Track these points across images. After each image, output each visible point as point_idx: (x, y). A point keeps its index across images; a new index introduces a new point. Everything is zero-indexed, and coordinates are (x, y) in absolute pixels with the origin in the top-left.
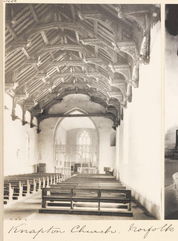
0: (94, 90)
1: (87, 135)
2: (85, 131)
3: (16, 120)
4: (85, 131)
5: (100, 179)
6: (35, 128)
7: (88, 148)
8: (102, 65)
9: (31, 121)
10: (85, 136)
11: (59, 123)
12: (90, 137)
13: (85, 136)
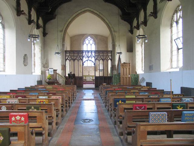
0: (135, 23)
1: (91, 42)
2: (89, 37)
3: (22, 16)
4: (89, 37)
5: (75, 17)
6: (41, 29)
7: (94, 54)
8: (178, 108)
9: (37, 21)
10: (89, 43)
11: (65, 30)
12: (95, 44)
13: (89, 43)
